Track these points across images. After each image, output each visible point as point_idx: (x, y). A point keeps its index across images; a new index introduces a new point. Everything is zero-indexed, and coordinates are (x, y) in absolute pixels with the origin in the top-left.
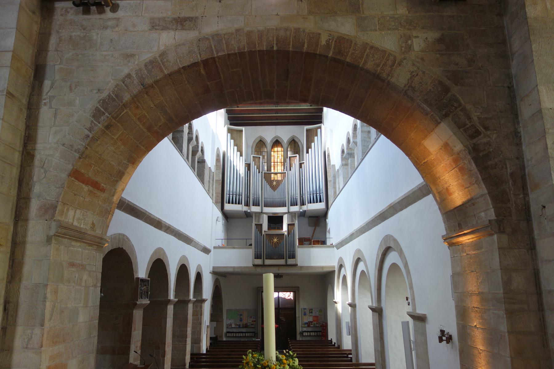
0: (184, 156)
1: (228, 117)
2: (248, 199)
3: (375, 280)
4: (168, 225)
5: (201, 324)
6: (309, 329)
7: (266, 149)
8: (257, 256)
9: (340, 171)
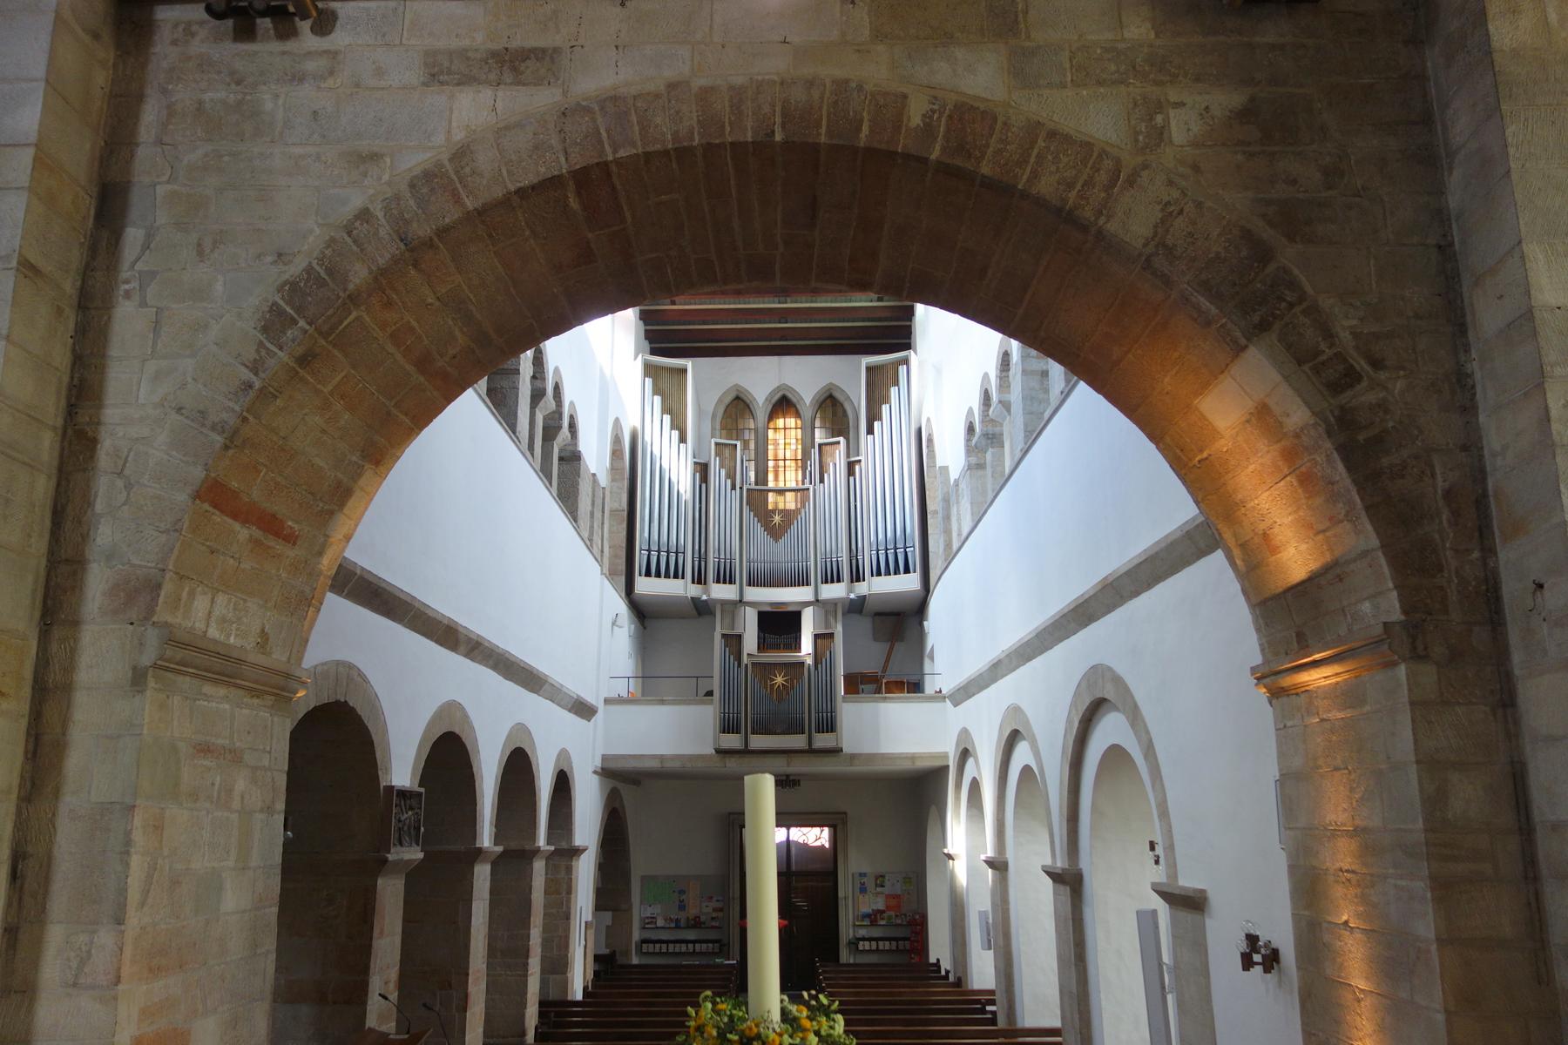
0: (520, 442)
1: (646, 331)
2: (703, 563)
3: (1061, 794)
4: (475, 638)
6: (876, 933)
7: (752, 420)
8: (728, 726)
9: (963, 486)
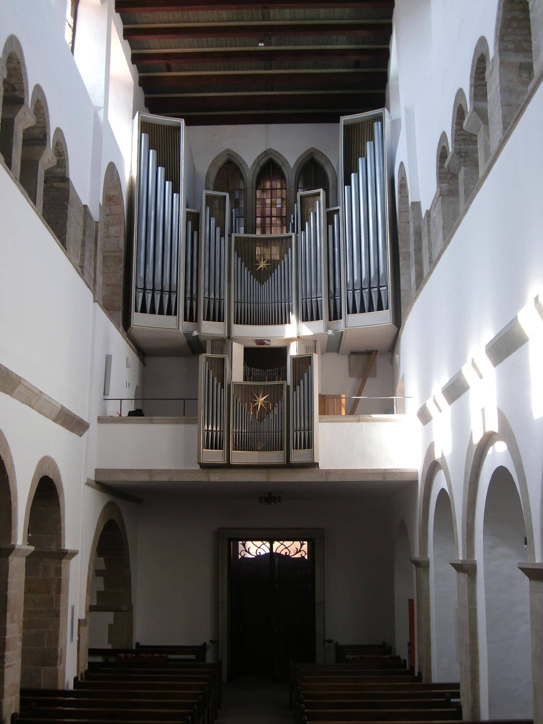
2: (194, 303)
5: (58, 616)
7: (241, 182)
9: (434, 215)
